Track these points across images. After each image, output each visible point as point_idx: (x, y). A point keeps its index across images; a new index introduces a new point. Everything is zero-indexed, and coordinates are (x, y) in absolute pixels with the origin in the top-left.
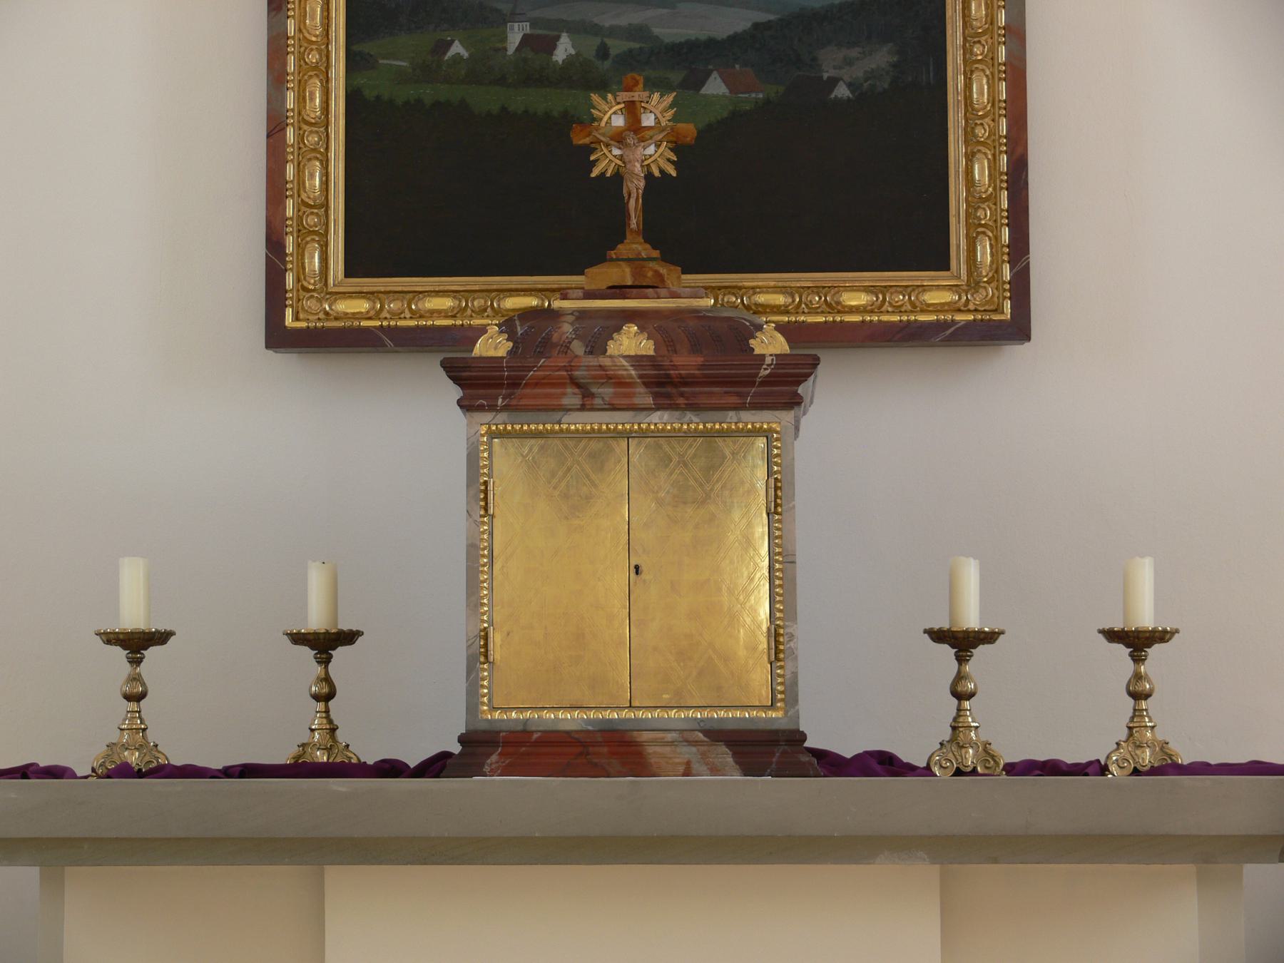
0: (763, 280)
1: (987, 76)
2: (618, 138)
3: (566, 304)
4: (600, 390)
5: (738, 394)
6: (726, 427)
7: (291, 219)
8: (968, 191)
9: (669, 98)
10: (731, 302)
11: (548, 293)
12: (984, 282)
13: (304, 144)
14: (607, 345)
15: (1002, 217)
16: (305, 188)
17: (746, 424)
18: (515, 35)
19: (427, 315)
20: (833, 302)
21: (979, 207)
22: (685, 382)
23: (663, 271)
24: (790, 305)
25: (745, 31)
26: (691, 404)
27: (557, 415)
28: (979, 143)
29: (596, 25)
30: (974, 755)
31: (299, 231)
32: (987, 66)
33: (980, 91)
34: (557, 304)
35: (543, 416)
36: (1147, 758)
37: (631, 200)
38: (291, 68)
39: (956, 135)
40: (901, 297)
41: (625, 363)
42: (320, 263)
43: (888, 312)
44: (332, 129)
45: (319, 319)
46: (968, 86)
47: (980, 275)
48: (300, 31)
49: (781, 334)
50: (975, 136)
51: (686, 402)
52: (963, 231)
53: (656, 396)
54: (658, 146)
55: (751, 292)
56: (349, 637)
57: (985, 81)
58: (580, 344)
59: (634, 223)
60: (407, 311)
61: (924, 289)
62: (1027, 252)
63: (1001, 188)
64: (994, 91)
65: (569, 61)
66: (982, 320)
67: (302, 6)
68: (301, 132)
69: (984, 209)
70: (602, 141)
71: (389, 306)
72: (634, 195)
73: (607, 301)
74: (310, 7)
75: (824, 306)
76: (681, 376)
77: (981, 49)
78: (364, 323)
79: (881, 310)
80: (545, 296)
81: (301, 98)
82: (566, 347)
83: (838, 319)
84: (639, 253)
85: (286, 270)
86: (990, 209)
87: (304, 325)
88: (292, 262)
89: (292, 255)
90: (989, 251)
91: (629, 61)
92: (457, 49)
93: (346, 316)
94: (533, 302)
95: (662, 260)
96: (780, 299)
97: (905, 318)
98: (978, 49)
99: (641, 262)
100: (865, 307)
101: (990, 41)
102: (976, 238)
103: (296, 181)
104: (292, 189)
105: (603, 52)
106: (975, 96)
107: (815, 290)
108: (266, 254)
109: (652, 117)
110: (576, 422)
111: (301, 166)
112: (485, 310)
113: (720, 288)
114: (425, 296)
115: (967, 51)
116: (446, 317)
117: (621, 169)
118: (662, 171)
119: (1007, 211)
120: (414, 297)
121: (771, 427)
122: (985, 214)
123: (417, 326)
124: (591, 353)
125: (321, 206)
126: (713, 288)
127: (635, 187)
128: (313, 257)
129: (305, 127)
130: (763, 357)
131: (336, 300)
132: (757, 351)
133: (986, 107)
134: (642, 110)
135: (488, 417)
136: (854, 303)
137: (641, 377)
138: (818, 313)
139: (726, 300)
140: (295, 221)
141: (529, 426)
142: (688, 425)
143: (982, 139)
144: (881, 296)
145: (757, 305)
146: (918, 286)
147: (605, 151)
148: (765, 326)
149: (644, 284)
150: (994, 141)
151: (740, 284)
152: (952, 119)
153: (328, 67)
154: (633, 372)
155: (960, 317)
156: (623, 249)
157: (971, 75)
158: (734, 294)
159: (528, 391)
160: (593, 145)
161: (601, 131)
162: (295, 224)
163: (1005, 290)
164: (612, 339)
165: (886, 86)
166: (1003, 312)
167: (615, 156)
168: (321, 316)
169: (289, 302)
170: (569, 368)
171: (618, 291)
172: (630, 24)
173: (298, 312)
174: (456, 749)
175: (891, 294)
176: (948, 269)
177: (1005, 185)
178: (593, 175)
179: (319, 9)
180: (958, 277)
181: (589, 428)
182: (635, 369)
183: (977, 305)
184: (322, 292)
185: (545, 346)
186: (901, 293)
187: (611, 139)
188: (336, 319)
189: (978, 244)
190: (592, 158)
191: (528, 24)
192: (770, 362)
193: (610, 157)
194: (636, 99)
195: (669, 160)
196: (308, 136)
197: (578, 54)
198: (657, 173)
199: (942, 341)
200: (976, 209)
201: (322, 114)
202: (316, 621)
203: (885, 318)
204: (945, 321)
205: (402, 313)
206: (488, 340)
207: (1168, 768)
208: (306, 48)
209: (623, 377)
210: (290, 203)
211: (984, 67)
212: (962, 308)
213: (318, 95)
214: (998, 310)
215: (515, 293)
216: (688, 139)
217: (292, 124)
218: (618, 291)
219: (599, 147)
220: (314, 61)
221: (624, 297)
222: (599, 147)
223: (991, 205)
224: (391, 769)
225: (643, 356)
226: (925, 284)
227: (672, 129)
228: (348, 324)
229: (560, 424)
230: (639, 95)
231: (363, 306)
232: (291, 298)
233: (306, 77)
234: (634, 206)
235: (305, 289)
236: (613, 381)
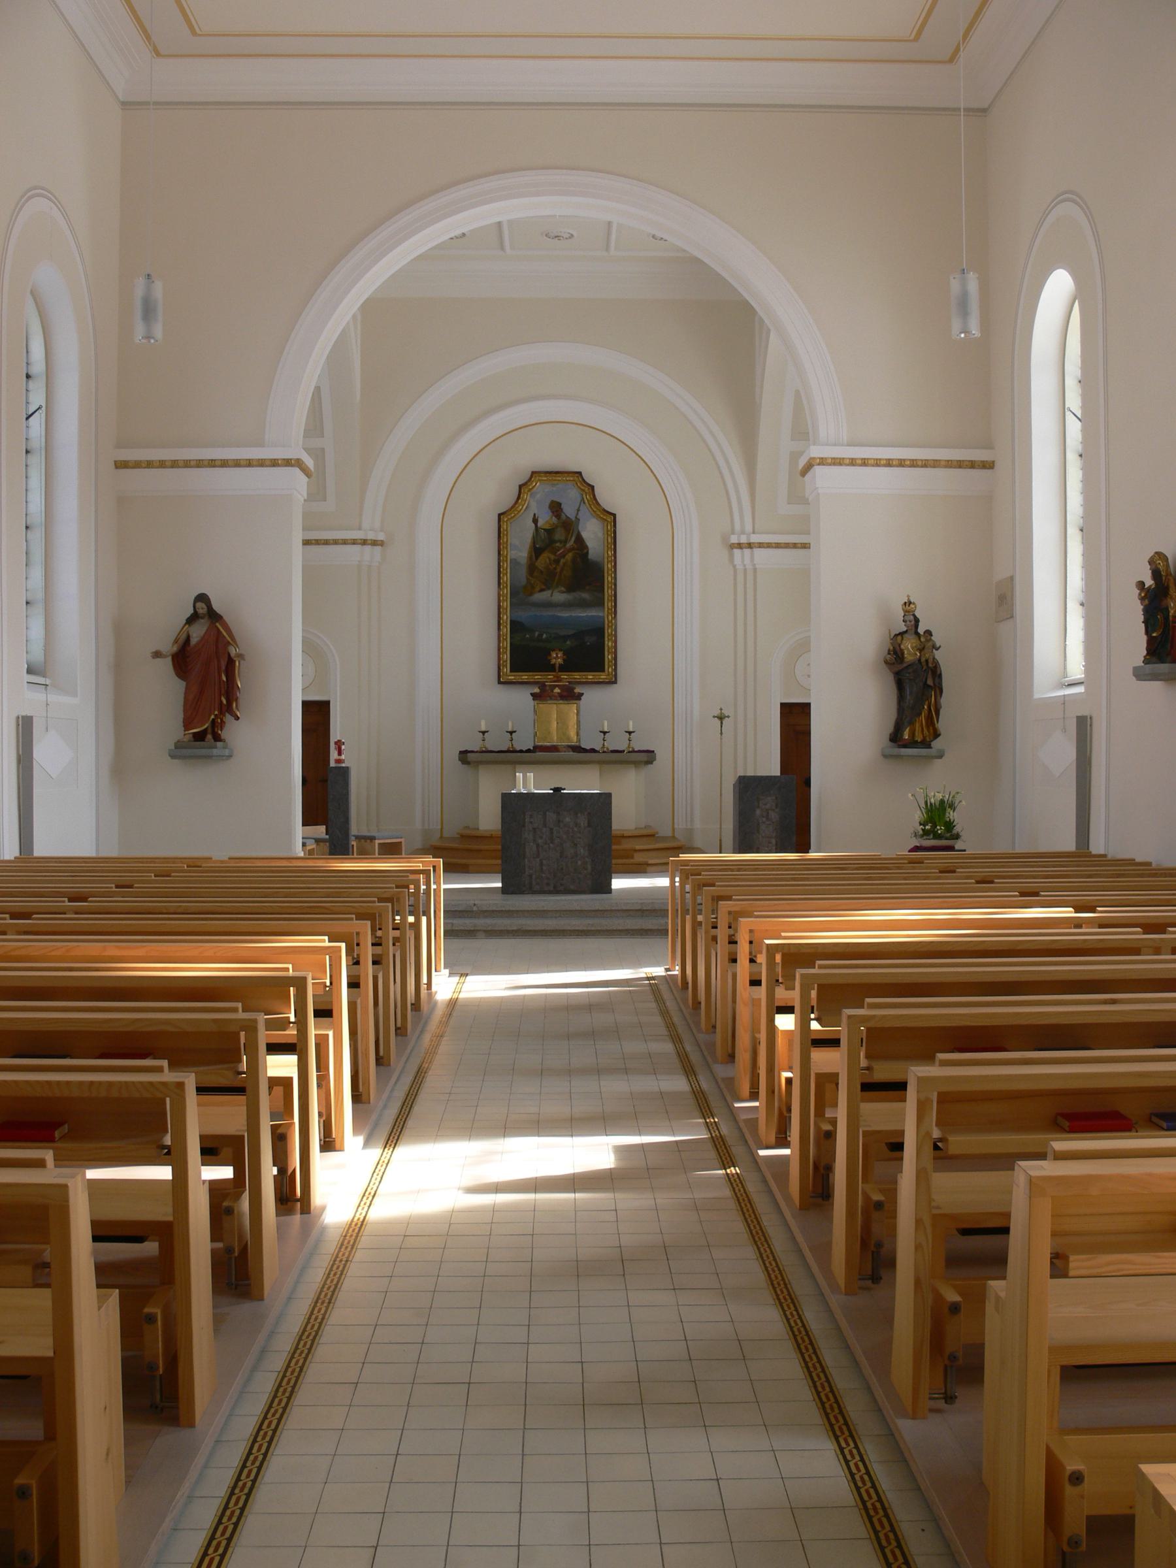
2: (555, 658)
18: (537, 634)
30: (1161, 617)
33: (610, 644)
36: (631, 749)
56: (515, 732)
92: (527, 636)
96: (578, 677)
105: (550, 637)
110: (549, 702)
127: (557, 666)
174: (532, 748)
202: (510, 730)
207: (634, 751)
224: (521, 751)
231: (513, 677)
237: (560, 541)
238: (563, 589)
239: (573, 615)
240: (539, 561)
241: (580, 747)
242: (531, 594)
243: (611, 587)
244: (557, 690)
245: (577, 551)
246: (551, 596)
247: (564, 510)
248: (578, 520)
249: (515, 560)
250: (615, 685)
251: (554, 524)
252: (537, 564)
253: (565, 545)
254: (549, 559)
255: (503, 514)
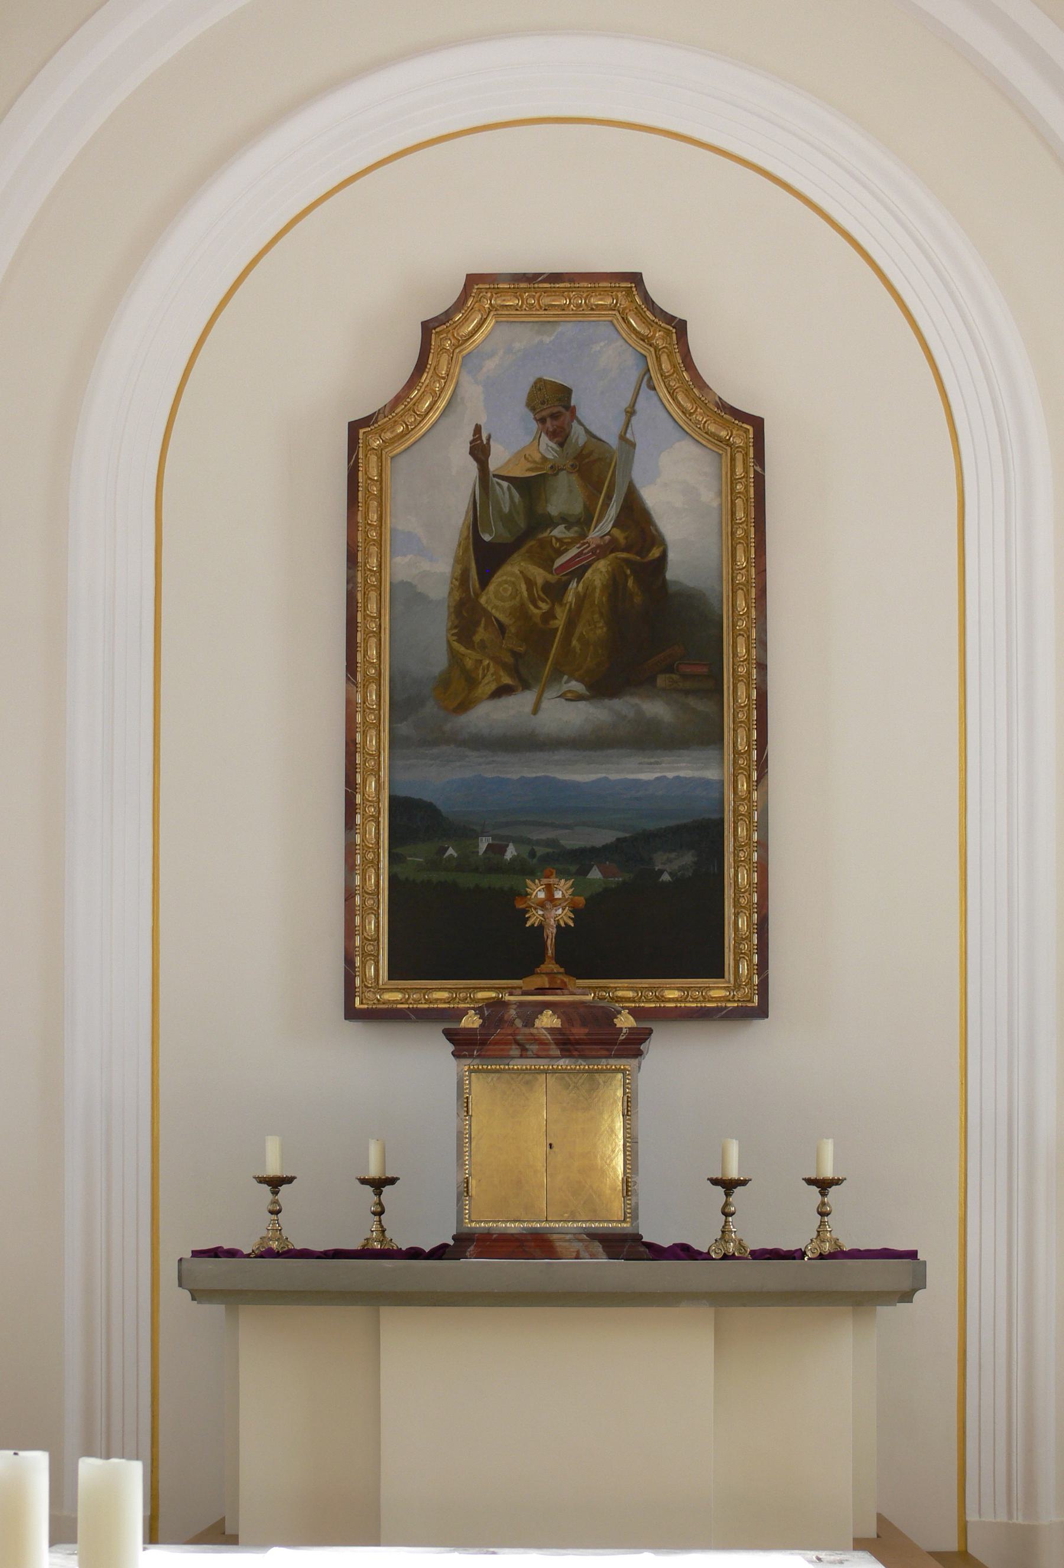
2: (542, 905)
18: (483, 844)
36: (827, 1248)
56: (392, 1181)
96: (630, 994)
105: (532, 854)
110: (517, 1064)
127: (551, 932)
174: (452, 1243)
224: (415, 1254)
231: (398, 996)
237: (565, 520)
238: (576, 686)
239: (613, 777)
240: (491, 588)
241: (637, 1238)
242: (464, 707)
243: (749, 673)
244: (548, 1020)
245: (624, 555)
246: (536, 710)
247: (581, 413)
248: (628, 444)
249: (408, 586)
250: (760, 1024)
251: (544, 459)
252: (483, 600)
253: (584, 536)
254: (530, 583)
255: (366, 422)
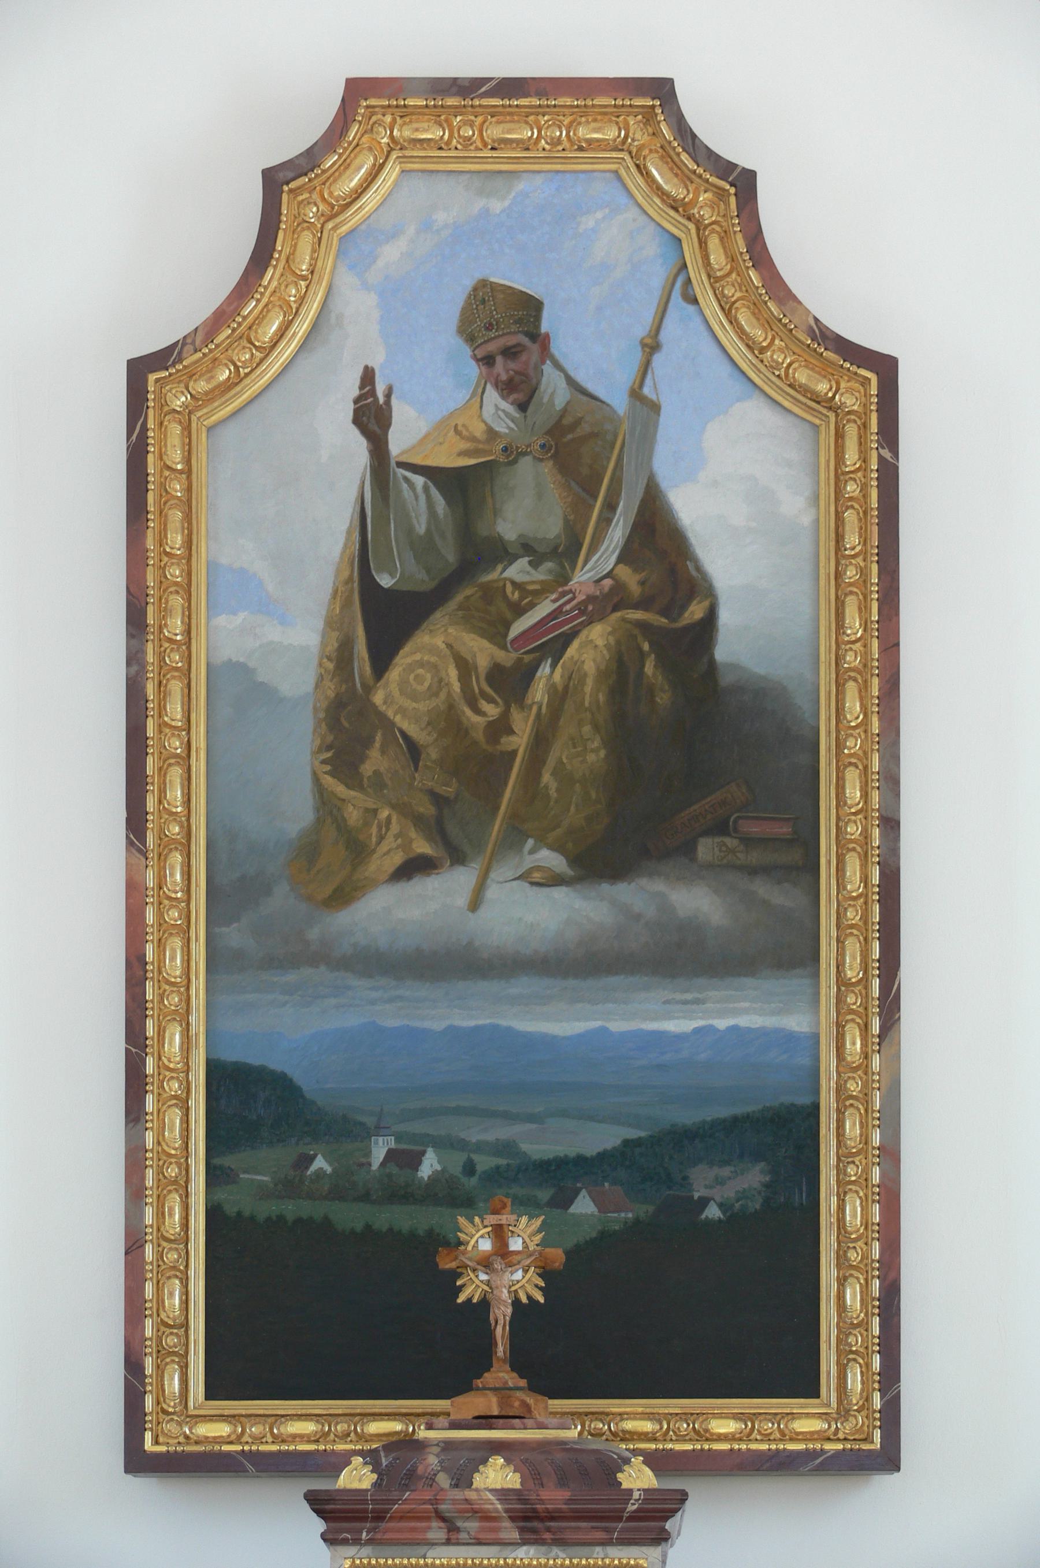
0: (631, 1406)
1: (860, 1198)
2: (485, 1263)
3: (432, 1434)
4: (467, 1524)
5: (606, 1530)
6: (592, 1562)
7: (151, 1339)
8: (839, 1316)
9: (538, 1222)
10: (598, 1429)
11: (412, 1418)
12: (855, 1410)
13: (163, 1261)
14: (472, 1477)
15: (873, 1344)
16: (164, 1307)
17: (613, 1560)
18: (379, 1150)
19: (290, 1439)
20: (701, 1430)
21: (850, 1333)
22: (552, 1516)
23: (530, 1401)
24: (657, 1432)
25: (614, 1148)
26: (555, 1539)
27: (422, 1550)
28: (852, 1267)
29: (464, 1139)
31: (159, 1352)
32: (861, 1188)
34: (423, 1434)
35: (407, 1549)
37: (498, 1327)
38: (149, 1182)
39: (828, 1258)
40: (770, 1425)
41: (491, 1497)
42: (180, 1384)
43: (756, 1440)
44: (191, 1246)
45: (179, 1443)
46: (841, 1208)
47: (850, 1403)
48: (159, 1143)
49: (649, 1467)
50: (848, 1259)
51: (552, 1537)
52: (833, 1358)
53: (522, 1530)
54: (526, 1271)
55: (618, 1418)
57: (858, 1202)
58: (446, 1476)
59: (501, 1349)
60: (268, 1435)
61: (793, 1416)
62: (898, 1380)
63: (873, 1314)
64: (867, 1214)
65: (435, 1178)
66: (851, 1450)
67: (161, 1118)
68: (160, 1249)
69: (855, 1335)
70: (468, 1266)
71: (250, 1430)
72: (501, 1322)
73: (473, 1431)
74: (169, 1118)
75: (692, 1433)
76: (547, 1510)
77: (855, 1169)
78: (226, 1448)
79: (750, 1438)
80: (408, 1420)
81: (160, 1213)
82: (431, 1480)
83: (706, 1447)
84: (506, 1383)
85: (145, 1393)
86: (862, 1336)
87: (163, 1449)
88: (151, 1384)
89: (151, 1376)
90: (859, 1378)
91: (495, 1177)
93: (206, 1440)
94: (397, 1426)
95: (529, 1390)
96: (648, 1426)
97: (773, 1447)
98: (852, 1170)
99: (507, 1391)
100: (733, 1434)
101: (864, 1161)
102: (847, 1365)
103: (155, 1300)
104: (151, 1308)
105: (470, 1169)
106: (848, 1218)
107: (683, 1417)
108: (125, 1375)
109: (520, 1241)
111: (160, 1285)
112: (348, 1435)
113: (587, 1414)
114: (287, 1420)
115: (841, 1171)
116: (309, 1442)
117: (487, 1295)
118: (529, 1297)
119: (879, 1338)
120: (276, 1421)
121: (638, 1563)
122: (856, 1341)
123: (280, 1451)
124: (456, 1486)
125: (181, 1326)
126: (580, 1414)
127: (502, 1313)
128: (173, 1379)
129: (164, 1244)
130: (630, 1491)
131: (196, 1423)
132: (625, 1486)
133: (858, 1230)
134: (510, 1234)
135: (352, 1550)
136: (722, 1431)
137: (507, 1511)
138: (685, 1440)
139: (592, 1426)
140: (154, 1341)
141: (393, 1560)
142: (554, 1560)
143: (855, 1263)
144: (749, 1424)
145: (624, 1431)
146: (788, 1414)
147: (472, 1275)
148: (633, 1460)
149: (511, 1414)
150: (866, 1265)
151: (608, 1410)
152: (824, 1242)
153: (187, 1182)
154: (499, 1506)
155: (829, 1446)
156: (489, 1378)
157: (845, 1196)
158: (602, 1421)
159: (391, 1525)
160: (459, 1270)
161: (467, 1256)
162: (154, 1345)
163: (875, 1419)
164: (479, 1471)
165: (758, 1207)
166: (872, 1442)
167: (482, 1282)
168: (182, 1439)
169: (148, 1425)
170: (434, 1502)
171: (485, 1421)
172: (497, 1139)
173: (157, 1436)
175: (760, 1421)
176: (818, 1397)
177: (877, 1311)
178: (459, 1301)
179: (178, 1121)
180: (828, 1405)
181: (454, 1562)
182: (500, 1504)
183: (847, 1434)
184: (182, 1415)
185: (410, 1478)
186: (770, 1420)
187: (478, 1264)
188: (197, 1443)
189: (849, 1371)
190: (459, 1283)
191: (393, 1138)
192: (638, 1497)
193: (477, 1282)
194: (504, 1222)
195: (536, 1286)
196: (167, 1253)
197: (443, 1171)
198: (524, 1299)
199: (809, 1470)
200: (848, 1335)
201: (182, 1230)
203: (754, 1446)
204: (814, 1450)
205: (263, 1437)
206: (352, 1471)
208: (165, 1162)
209: (488, 1511)
210: (148, 1322)
211: (858, 1189)
212: (832, 1437)
213: (177, 1211)
214: (868, 1439)
215: (379, 1417)
216: (557, 1264)
217: (151, 1241)
218: (483, 1421)
219: (465, 1272)
220: (173, 1175)
221: (491, 1427)
222: (465, 1272)
223: (862, 1331)
225: (509, 1490)
226: (795, 1411)
227: (540, 1254)
228: (209, 1448)
229: (425, 1559)
230: (507, 1219)
231: (223, 1429)
232: (151, 1422)
233: (165, 1192)
234: (501, 1333)
235: (165, 1412)
236: (479, 1515)
